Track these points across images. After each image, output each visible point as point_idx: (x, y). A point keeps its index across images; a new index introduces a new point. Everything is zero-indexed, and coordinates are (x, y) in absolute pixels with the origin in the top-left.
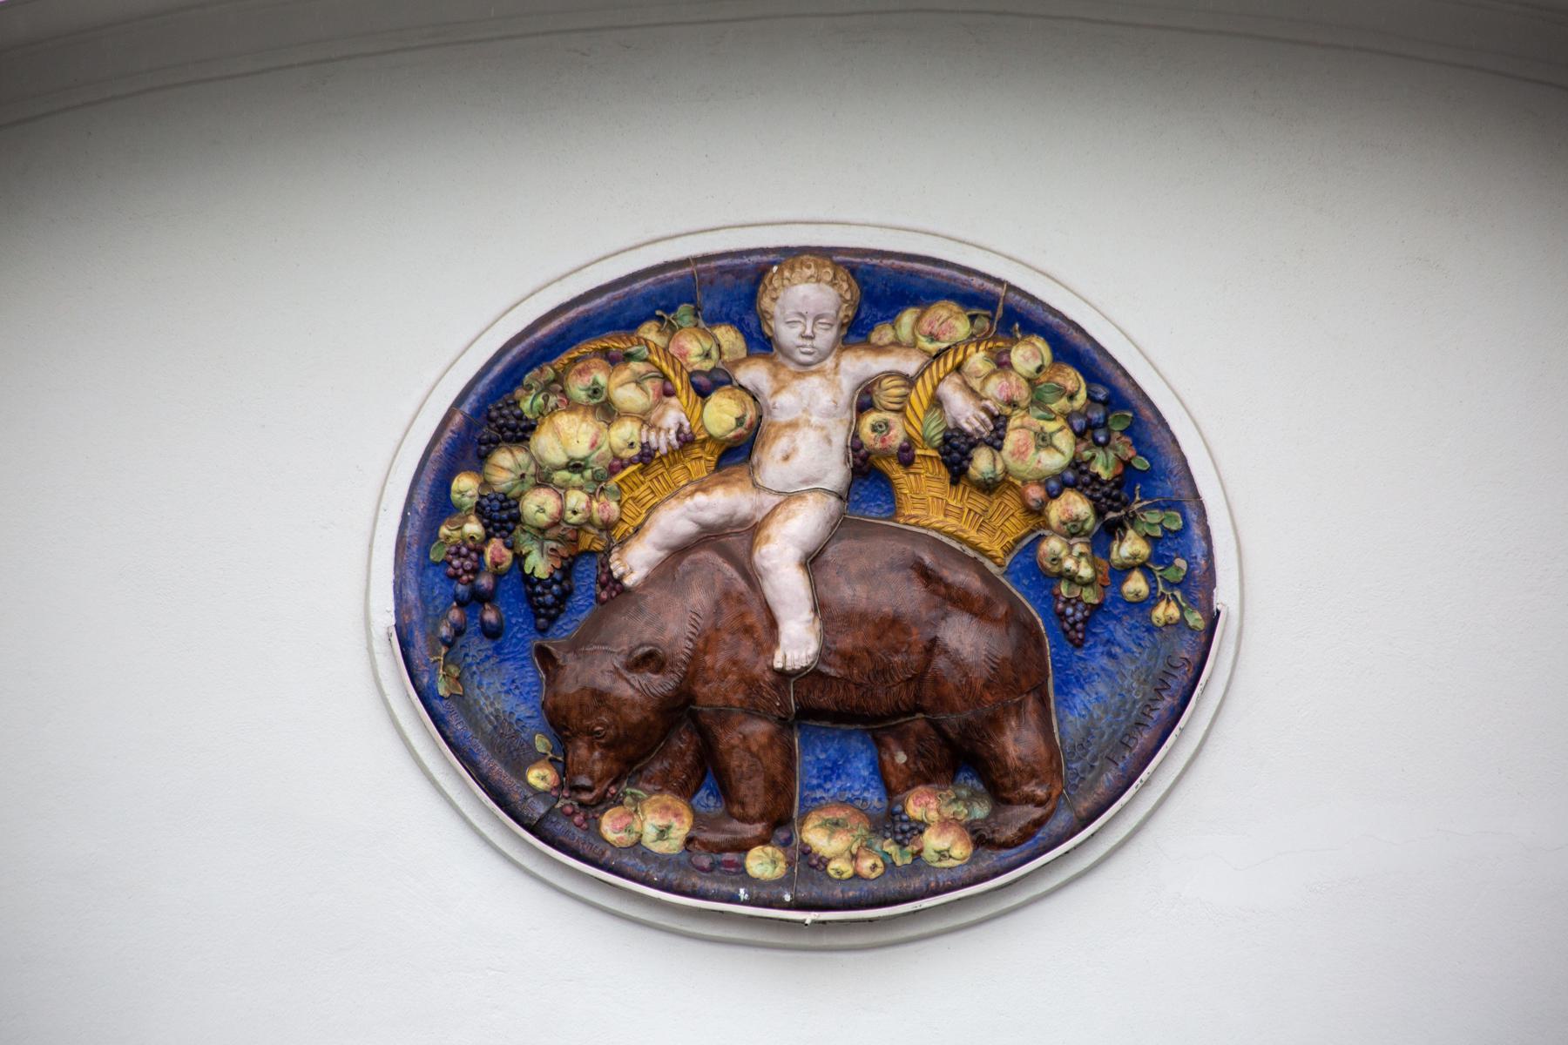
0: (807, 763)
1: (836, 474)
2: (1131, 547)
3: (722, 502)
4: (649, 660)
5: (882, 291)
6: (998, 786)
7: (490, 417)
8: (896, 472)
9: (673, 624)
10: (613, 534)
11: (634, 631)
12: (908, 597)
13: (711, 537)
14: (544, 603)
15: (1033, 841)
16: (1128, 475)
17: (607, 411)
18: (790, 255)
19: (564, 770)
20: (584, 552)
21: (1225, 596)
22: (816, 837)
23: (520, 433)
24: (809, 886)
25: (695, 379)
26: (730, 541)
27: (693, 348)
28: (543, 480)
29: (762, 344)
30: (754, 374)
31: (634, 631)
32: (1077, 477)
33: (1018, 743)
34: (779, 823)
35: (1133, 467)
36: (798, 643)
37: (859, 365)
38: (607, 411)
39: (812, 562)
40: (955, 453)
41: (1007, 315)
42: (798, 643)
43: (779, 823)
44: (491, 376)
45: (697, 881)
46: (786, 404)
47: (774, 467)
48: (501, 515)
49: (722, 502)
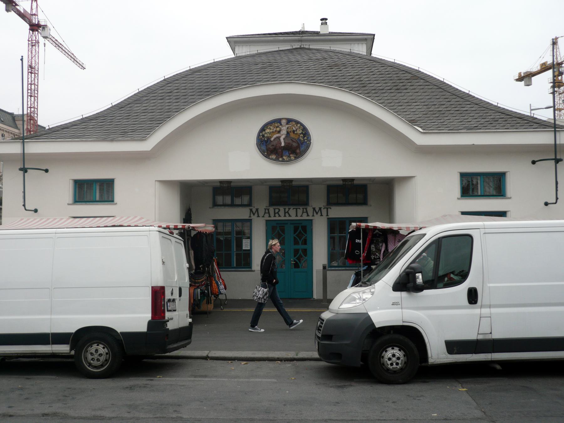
0: (284, 152)
1: (286, 133)
2: (305, 138)
3: (278, 135)
4: (273, 146)
5: (289, 121)
6: (296, 154)
7: (263, 129)
8: (462, 289)
9: (275, 143)
10: (271, 137)
11: (272, 144)
12: (290, 141)
13: (302, 251)
14: (266, 142)
15: (298, 157)
16: (305, 133)
17: (270, 129)
18: (283, 119)
19: (267, 153)
20: (269, 138)
21: (312, 141)
22: (284, 158)
23: (265, 130)
24: (283, 161)
25: (229, 39)
26: (279, 138)
27: (276, 125)
28: (266, 133)
29: (281, 125)
30: (280, 127)
31: (272, 144)
32: (302, 133)
33: (298, 151)
34: (282, 157)
35: (306, 133)
36: (283, 144)
37: (287, 126)
38: (270, 129)
39: (284, 139)
40: (294, 131)
41: (297, 122)
42: (283, 144)
43: (282, 157)
44: (65, 360)
45: (276, 160)
46: (282, 128)
47: (282, 133)
48: (263, 136)
49: (278, 135)
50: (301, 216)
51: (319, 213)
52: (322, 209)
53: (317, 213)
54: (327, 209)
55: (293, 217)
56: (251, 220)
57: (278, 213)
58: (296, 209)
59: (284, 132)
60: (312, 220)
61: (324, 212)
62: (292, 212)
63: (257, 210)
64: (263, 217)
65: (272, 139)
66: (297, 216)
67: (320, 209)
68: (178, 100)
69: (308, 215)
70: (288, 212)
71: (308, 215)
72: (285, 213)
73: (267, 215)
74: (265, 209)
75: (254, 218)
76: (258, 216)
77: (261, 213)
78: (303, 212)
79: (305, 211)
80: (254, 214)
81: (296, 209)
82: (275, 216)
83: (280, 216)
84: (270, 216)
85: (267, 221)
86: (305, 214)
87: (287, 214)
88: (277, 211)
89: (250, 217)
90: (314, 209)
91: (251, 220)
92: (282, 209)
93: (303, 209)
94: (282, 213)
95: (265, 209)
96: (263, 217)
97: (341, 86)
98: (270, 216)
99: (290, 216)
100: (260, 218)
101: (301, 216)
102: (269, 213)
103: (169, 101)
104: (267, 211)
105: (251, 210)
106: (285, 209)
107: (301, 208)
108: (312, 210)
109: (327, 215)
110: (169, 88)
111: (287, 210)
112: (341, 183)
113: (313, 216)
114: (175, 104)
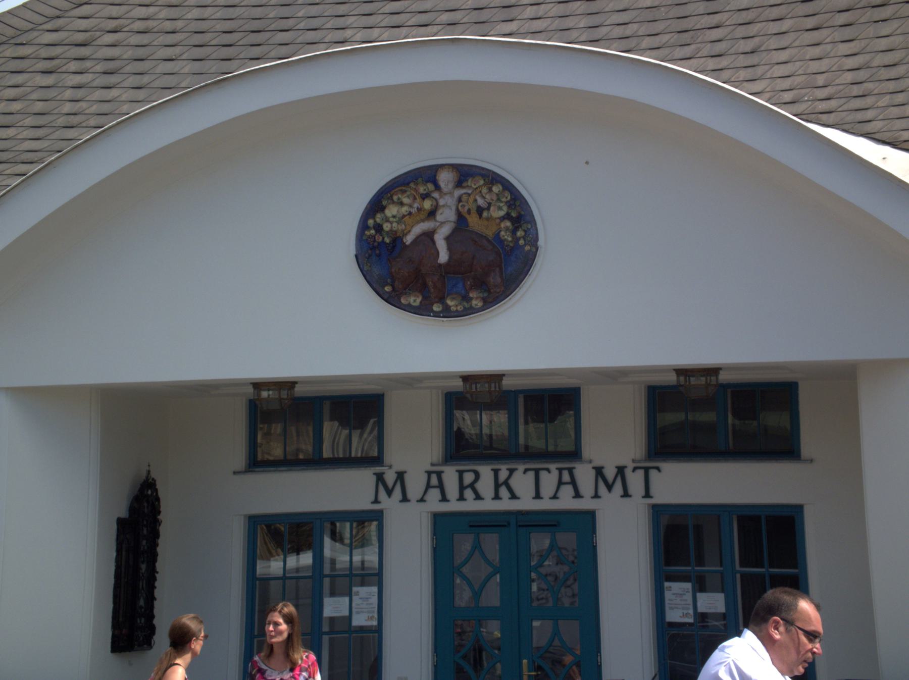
2: (520, 233)
5: (465, 174)
7: (376, 206)
17: (402, 204)
18: (442, 166)
20: (397, 239)
21: (541, 243)
22: (450, 302)
23: (382, 209)
24: (447, 313)
26: (429, 235)
28: (387, 220)
29: (437, 187)
30: (436, 195)
32: (507, 217)
34: (442, 300)
35: (520, 214)
39: (448, 239)
40: (480, 210)
41: (492, 178)
42: (443, 257)
43: (442, 300)
45: (422, 310)
46: (442, 202)
47: (439, 217)
48: (379, 228)
50: (555, 497)
51: (618, 488)
52: (628, 472)
53: (610, 487)
54: (647, 470)
55: (526, 503)
56: (381, 512)
57: (472, 486)
58: (537, 472)
59: (447, 214)
60: (592, 514)
61: (635, 481)
62: (523, 482)
63: (401, 476)
64: (422, 500)
65: (409, 239)
66: (538, 496)
67: (621, 470)
68: (113, 79)
69: (578, 495)
70: (506, 483)
71: (578, 495)
72: (497, 486)
73: (435, 494)
74: (429, 473)
75: (390, 504)
76: (405, 499)
77: (415, 484)
78: (560, 483)
79: (566, 477)
80: (389, 492)
81: (537, 472)
82: (461, 498)
83: (478, 497)
84: (444, 499)
85: (437, 518)
86: (567, 490)
87: (469, 493)
88: (469, 478)
89: (376, 501)
90: (599, 471)
91: (381, 512)
92: (486, 471)
93: (560, 470)
94: (486, 485)
95: (429, 473)
96: (422, 500)
97: (632, 43)
98: (444, 499)
99: (514, 496)
100: (413, 507)
101: (555, 497)
102: (441, 486)
103: (78, 79)
104: (434, 481)
105: (380, 478)
106: (496, 472)
107: (553, 467)
108: (593, 472)
109: (647, 495)
110: (84, 24)
111: (503, 475)
112: (672, 379)
113: (596, 496)
114: (99, 94)
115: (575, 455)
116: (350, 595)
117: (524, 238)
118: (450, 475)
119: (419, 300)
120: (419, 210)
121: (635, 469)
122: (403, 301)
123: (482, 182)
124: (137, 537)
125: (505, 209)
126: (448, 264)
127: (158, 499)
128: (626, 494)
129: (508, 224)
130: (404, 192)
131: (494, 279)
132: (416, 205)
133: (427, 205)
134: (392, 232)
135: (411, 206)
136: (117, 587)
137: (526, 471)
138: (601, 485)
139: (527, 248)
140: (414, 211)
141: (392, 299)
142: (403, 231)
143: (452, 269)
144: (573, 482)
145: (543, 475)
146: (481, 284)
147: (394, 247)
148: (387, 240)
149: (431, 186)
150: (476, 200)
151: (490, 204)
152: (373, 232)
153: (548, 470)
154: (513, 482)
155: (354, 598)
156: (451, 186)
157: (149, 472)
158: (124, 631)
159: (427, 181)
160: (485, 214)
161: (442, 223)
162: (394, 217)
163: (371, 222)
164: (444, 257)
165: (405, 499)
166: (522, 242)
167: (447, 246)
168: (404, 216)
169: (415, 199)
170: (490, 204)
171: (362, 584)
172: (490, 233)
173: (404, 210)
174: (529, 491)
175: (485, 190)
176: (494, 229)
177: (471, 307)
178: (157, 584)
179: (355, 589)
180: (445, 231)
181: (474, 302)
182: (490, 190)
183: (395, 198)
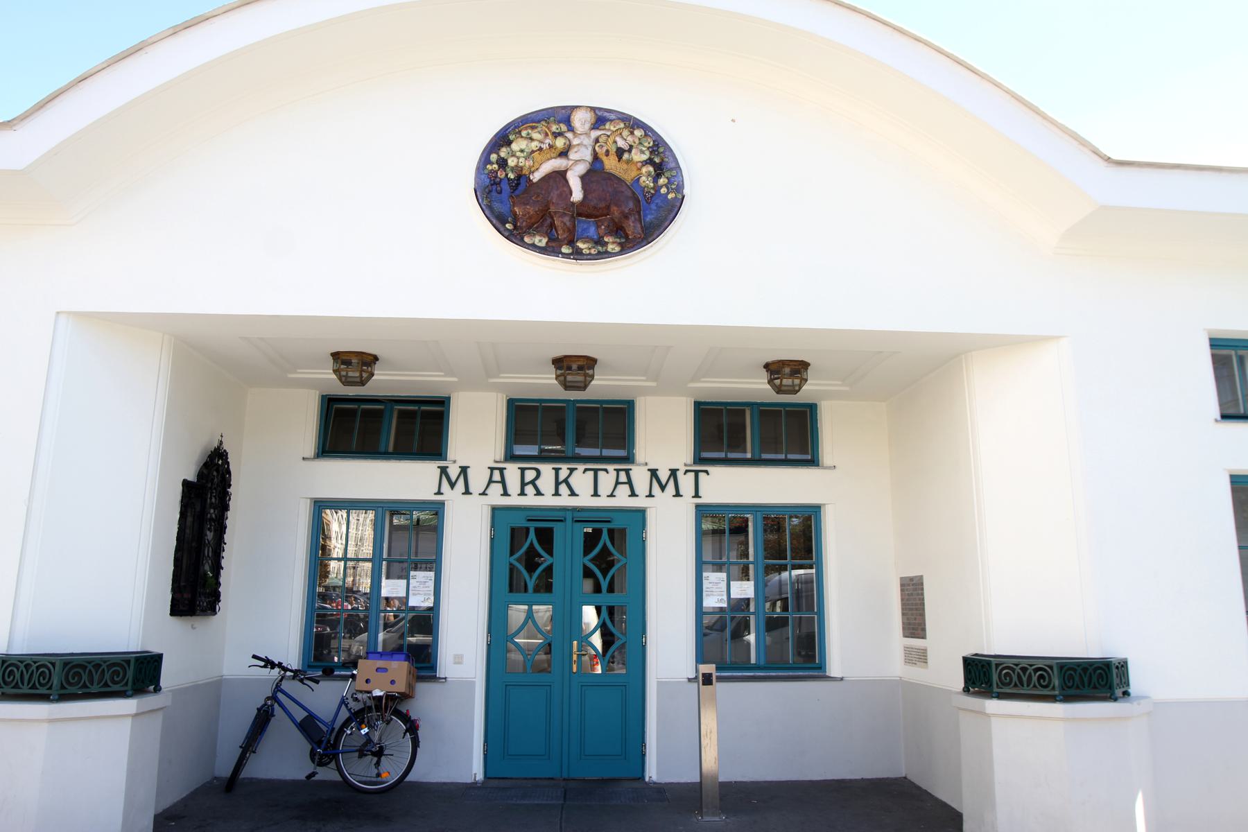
2: (662, 181)
7: (502, 139)
17: (532, 139)
22: (580, 245)
23: (509, 143)
24: (577, 255)
30: (569, 135)
32: (650, 161)
35: (661, 159)
39: (583, 178)
40: (620, 152)
41: (632, 123)
43: (571, 243)
45: (551, 249)
46: (575, 142)
47: (572, 155)
48: (503, 163)
50: (612, 495)
51: (671, 488)
52: (680, 475)
53: (663, 488)
54: (697, 473)
55: (585, 499)
56: (442, 504)
58: (596, 471)
61: (686, 482)
63: (464, 470)
64: (484, 494)
65: (536, 177)
66: (596, 494)
67: (674, 472)
70: (566, 481)
72: (557, 484)
73: (496, 489)
74: (492, 469)
75: (452, 497)
76: (467, 492)
77: (478, 479)
79: (623, 478)
80: (452, 485)
81: (596, 471)
83: (539, 493)
84: (505, 494)
85: (495, 509)
86: (624, 490)
88: (530, 475)
89: (439, 493)
90: (654, 473)
91: (442, 504)
92: (547, 469)
93: (618, 471)
96: (484, 494)
99: (573, 494)
100: (475, 498)
101: (612, 495)
104: (497, 476)
105: (444, 471)
106: (557, 470)
107: (611, 468)
109: (697, 495)
111: (563, 474)
115: (629, 459)
116: (408, 578)
117: (666, 185)
118: (512, 472)
119: (545, 240)
120: (551, 146)
121: (687, 471)
122: (527, 239)
123: (622, 125)
124: (204, 502)
125: (648, 153)
126: (582, 203)
127: (229, 473)
128: (678, 494)
129: (651, 169)
130: (533, 128)
131: (632, 227)
132: (547, 141)
133: (560, 143)
134: (518, 170)
135: (541, 142)
136: (178, 550)
137: (586, 470)
138: (655, 483)
139: (670, 196)
140: (545, 146)
141: (516, 236)
142: (530, 167)
143: (582, 211)
144: (630, 482)
145: (601, 474)
146: (617, 229)
147: (518, 184)
148: (511, 176)
149: (564, 127)
150: (615, 142)
151: (631, 147)
152: (496, 166)
153: (606, 470)
154: (571, 480)
155: (411, 581)
156: (588, 126)
157: (221, 443)
158: (186, 596)
159: (559, 122)
160: (626, 156)
161: (577, 161)
162: (522, 151)
163: (494, 157)
164: (577, 195)
165: (467, 492)
166: (664, 190)
167: (582, 194)
168: (533, 152)
169: (547, 135)
170: (631, 147)
171: (416, 569)
172: (628, 177)
173: (534, 145)
174: (587, 489)
175: (625, 133)
176: (634, 174)
177: (606, 252)
178: (224, 554)
179: (412, 573)
180: (581, 169)
181: (610, 247)
182: (632, 133)
183: (524, 133)
